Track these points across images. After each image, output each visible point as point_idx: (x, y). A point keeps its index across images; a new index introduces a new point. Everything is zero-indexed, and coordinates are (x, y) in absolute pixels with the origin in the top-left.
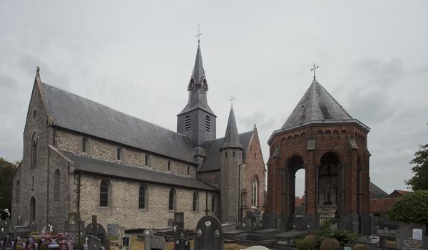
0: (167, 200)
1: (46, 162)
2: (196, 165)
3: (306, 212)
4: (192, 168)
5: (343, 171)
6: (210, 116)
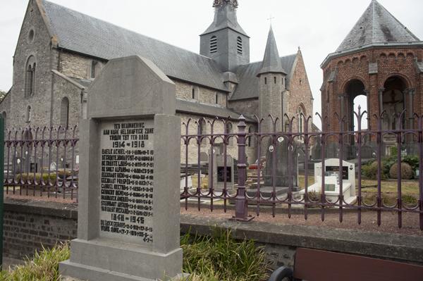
1: (50, 90)
2: (227, 93)
3: (370, 140)
4: (221, 96)
5: (411, 96)
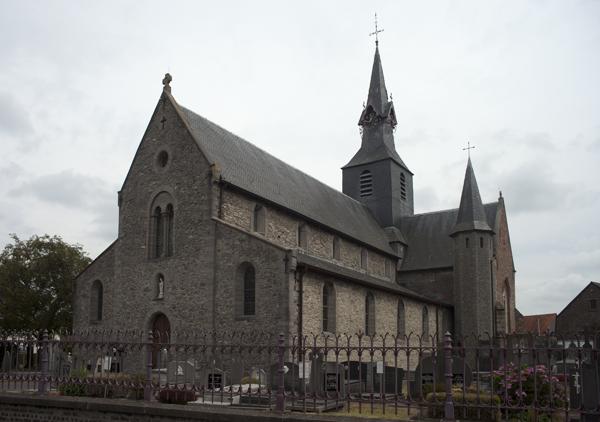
2: (395, 259)
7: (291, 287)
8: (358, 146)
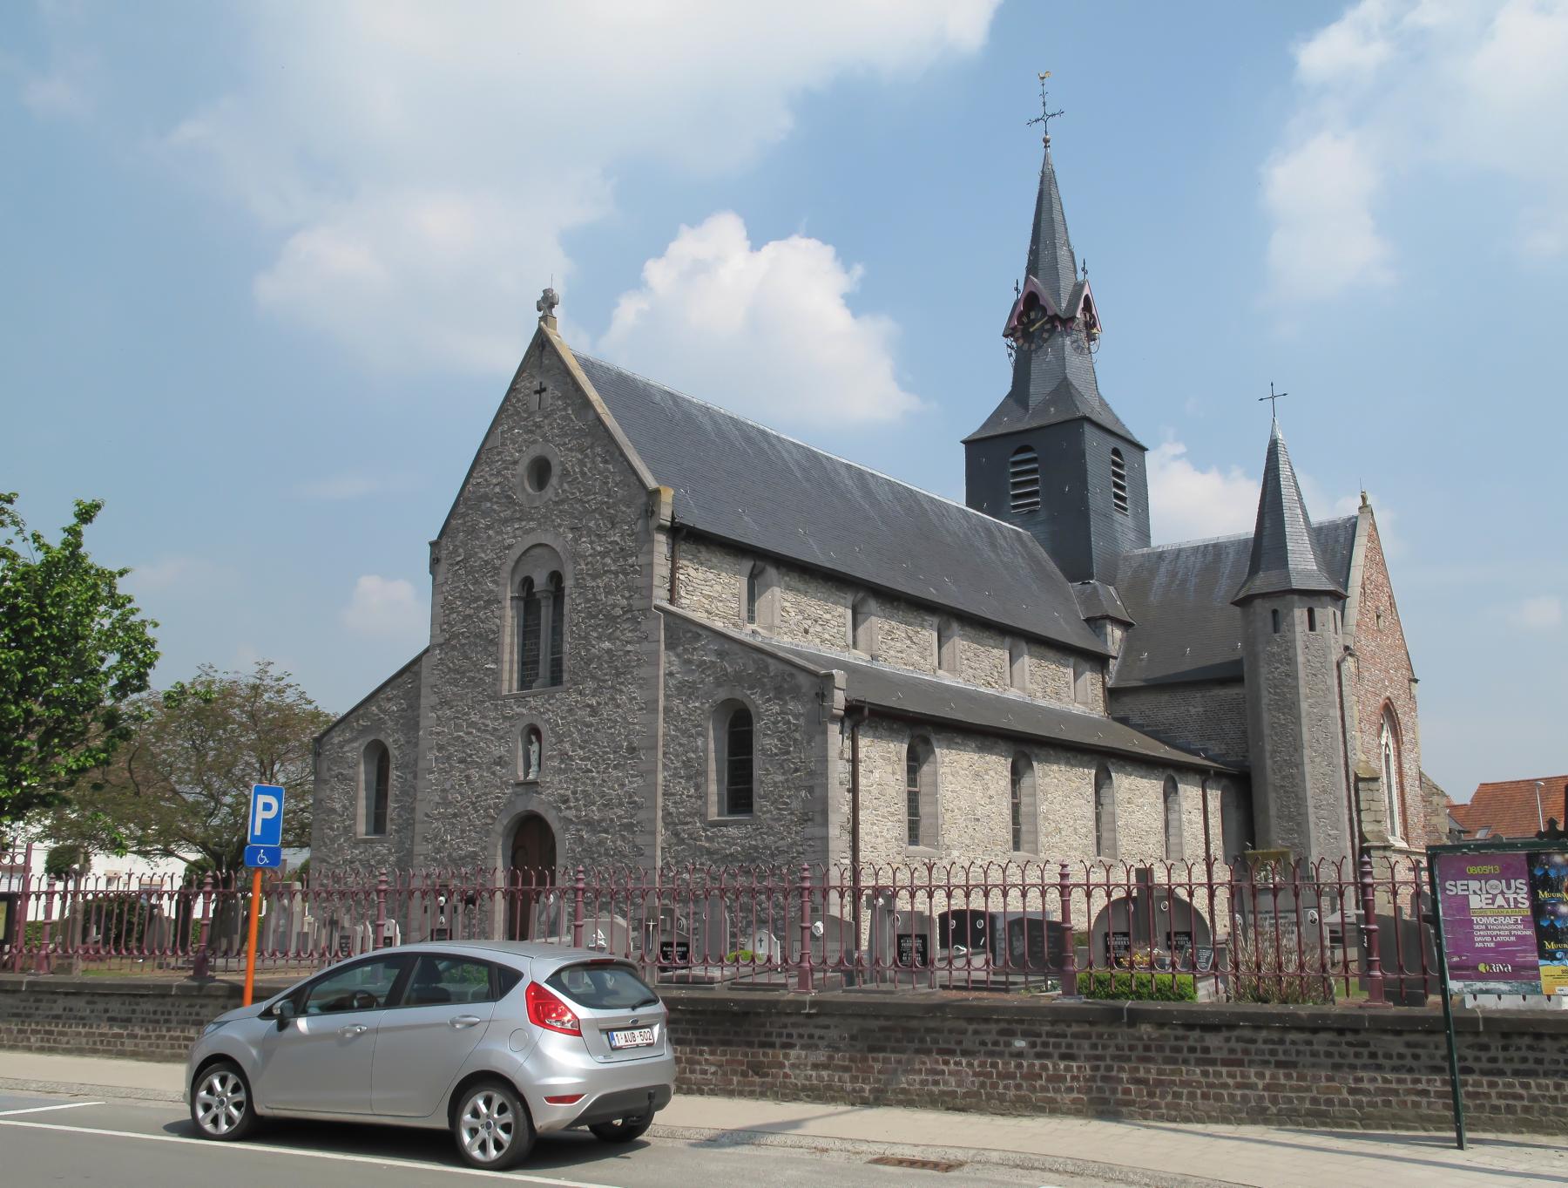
0: (1089, 810)
6: (1122, 447)
7: (833, 753)
8: (1009, 389)
